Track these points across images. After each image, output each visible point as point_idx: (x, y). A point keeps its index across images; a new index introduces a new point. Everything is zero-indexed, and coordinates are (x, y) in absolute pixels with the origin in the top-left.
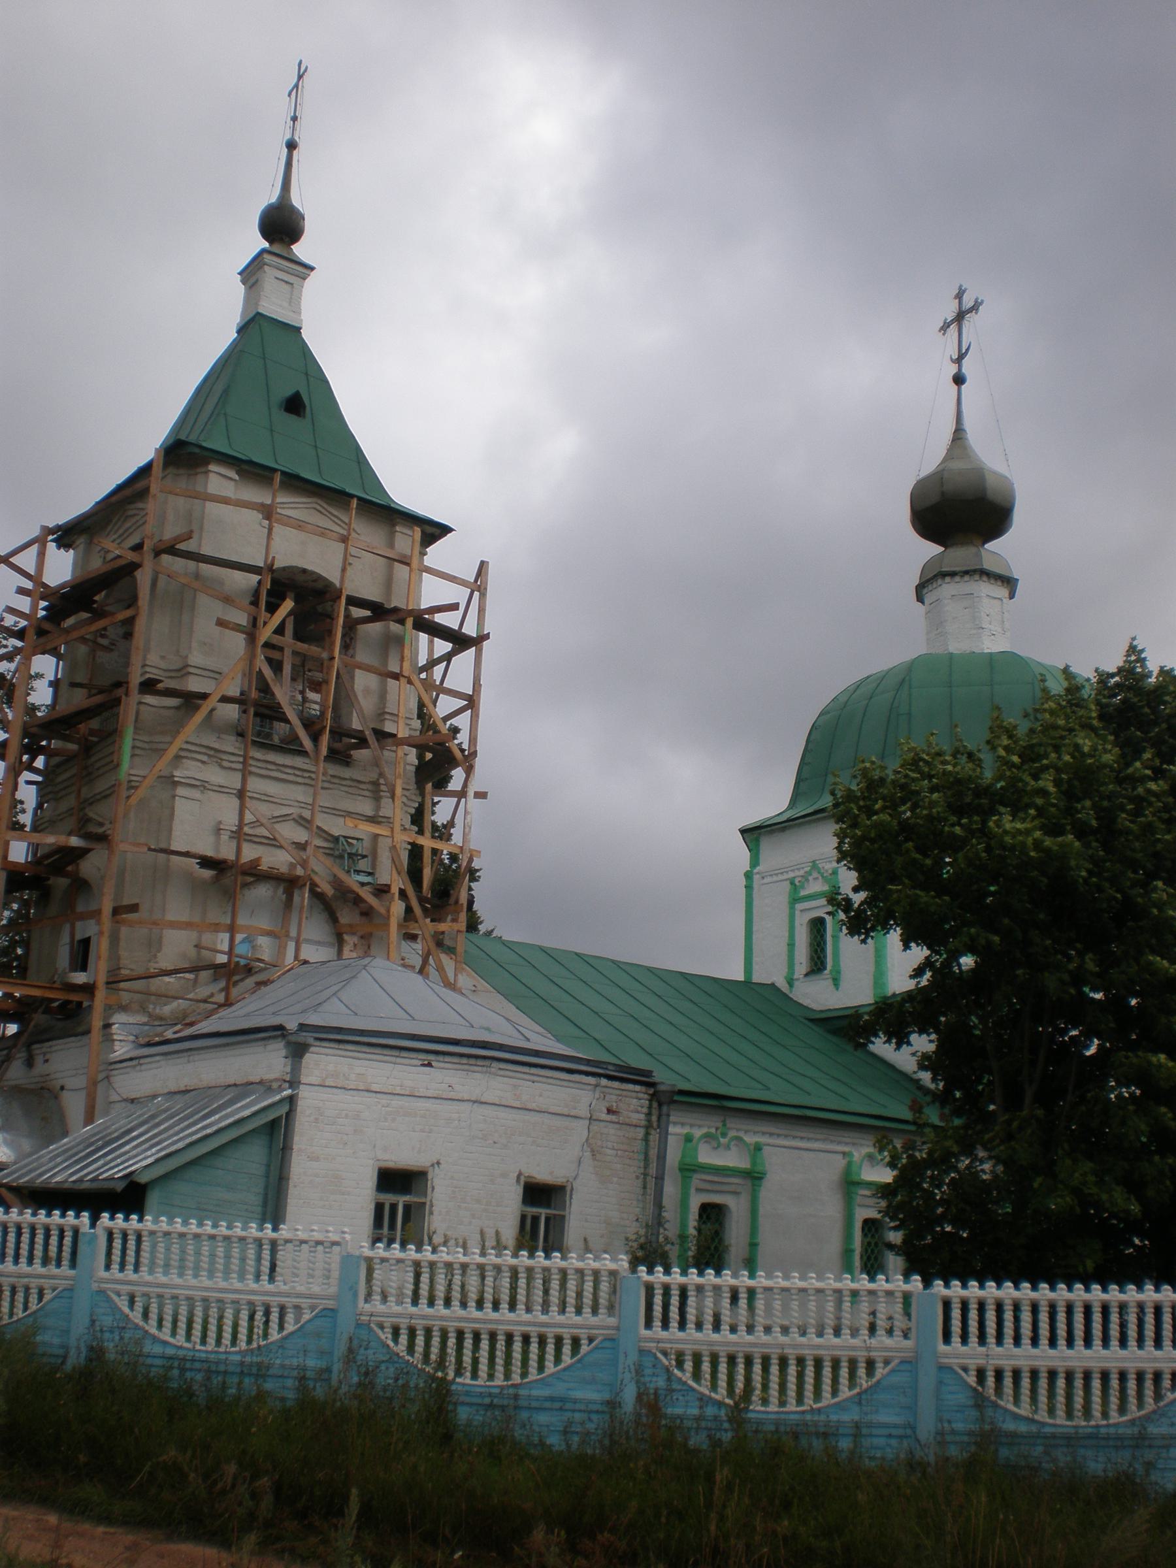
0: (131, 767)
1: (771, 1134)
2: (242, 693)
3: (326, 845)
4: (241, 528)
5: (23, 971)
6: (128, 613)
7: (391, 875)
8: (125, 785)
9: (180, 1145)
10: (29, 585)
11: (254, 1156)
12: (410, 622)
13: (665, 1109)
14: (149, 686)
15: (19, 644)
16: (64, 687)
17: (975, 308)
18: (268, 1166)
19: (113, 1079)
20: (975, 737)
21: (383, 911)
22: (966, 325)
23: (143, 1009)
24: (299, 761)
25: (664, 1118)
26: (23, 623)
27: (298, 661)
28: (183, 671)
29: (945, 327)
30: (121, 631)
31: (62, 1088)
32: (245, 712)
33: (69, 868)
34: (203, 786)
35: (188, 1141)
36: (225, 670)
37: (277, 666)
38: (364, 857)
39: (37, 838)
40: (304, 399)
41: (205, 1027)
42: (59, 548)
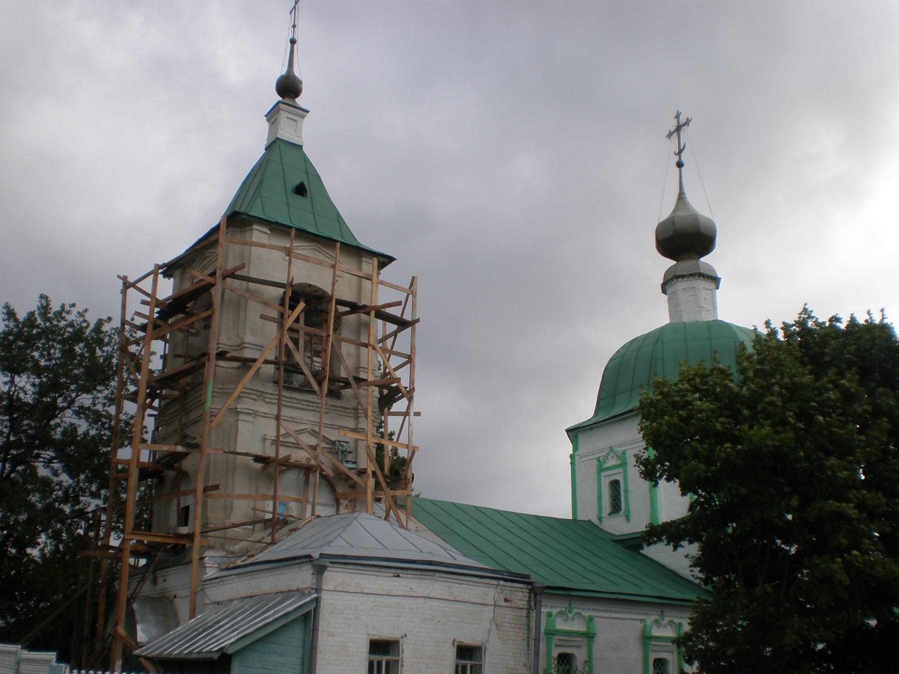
0: (212, 404)
1: (598, 610)
2: (276, 358)
3: (328, 446)
4: (272, 262)
5: (149, 528)
6: (208, 313)
7: (365, 462)
8: (209, 415)
9: (252, 630)
10: (149, 299)
11: (296, 636)
12: (373, 313)
13: (538, 597)
14: (221, 355)
15: (143, 334)
16: (169, 360)
17: (687, 123)
18: (304, 641)
19: (206, 590)
20: (727, 363)
21: (362, 484)
22: (682, 132)
23: (222, 548)
24: (310, 397)
25: (538, 603)
26: (145, 321)
27: (308, 339)
28: (241, 346)
29: (670, 135)
30: (202, 325)
31: (175, 596)
32: (278, 369)
33: (176, 465)
34: (255, 414)
35: (255, 627)
36: (266, 345)
37: (296, 342)
38: (350, 452)
39: (156, 447)
40: (304, 188)
41: (261, 557)
42: (164, 277)
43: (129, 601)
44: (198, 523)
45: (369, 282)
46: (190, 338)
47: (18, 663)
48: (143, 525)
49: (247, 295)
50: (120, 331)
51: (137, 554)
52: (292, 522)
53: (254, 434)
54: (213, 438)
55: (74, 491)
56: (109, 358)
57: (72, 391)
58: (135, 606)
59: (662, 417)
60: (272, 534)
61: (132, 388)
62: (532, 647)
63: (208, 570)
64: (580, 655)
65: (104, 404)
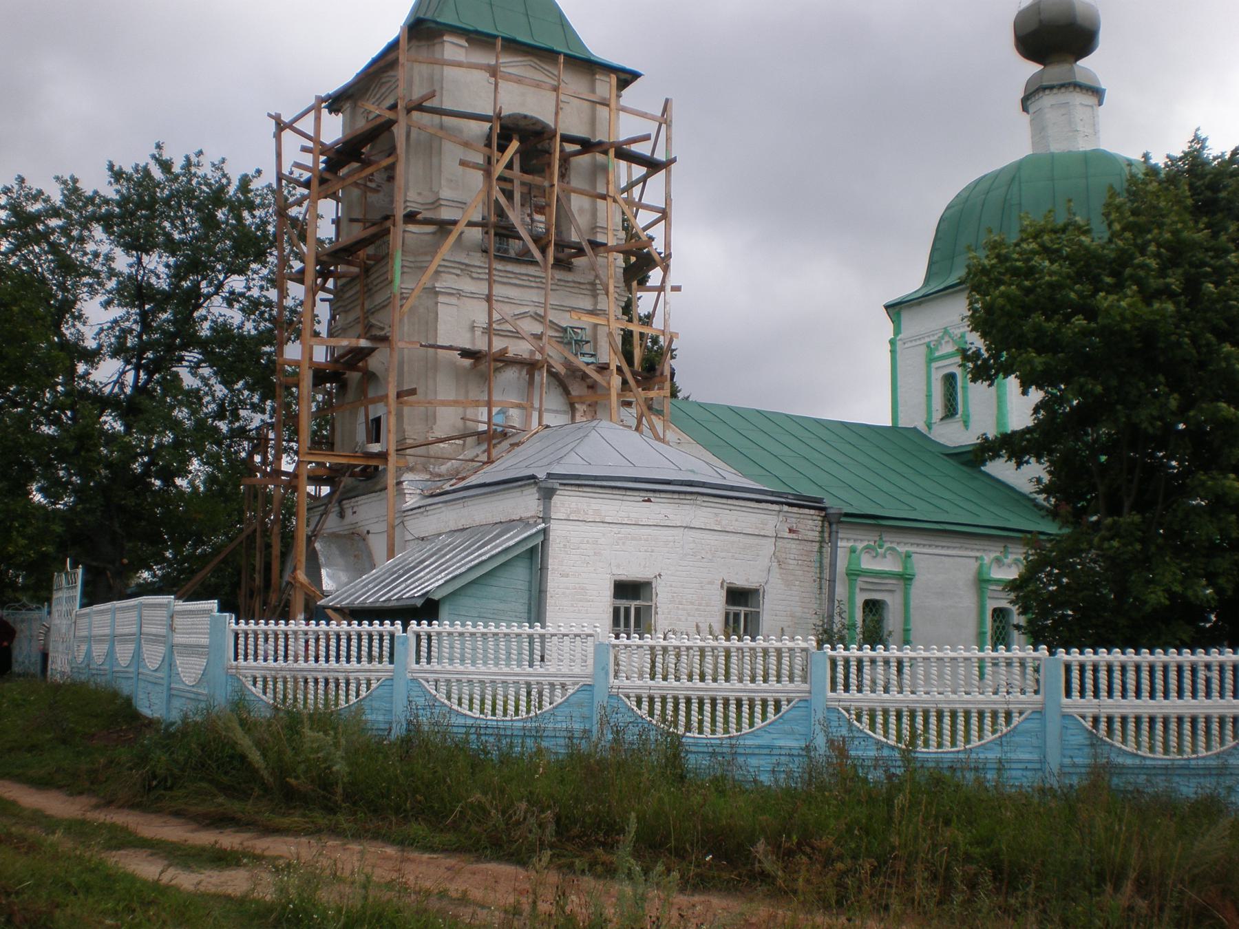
4: (474, 87)
5: (331, 445)
7: (609, 355)
9: (463, 569)
10: (310, 144)
11: (520, 575)
12: (612, 152)
13: (834, 526)
14: (411, 217)
15: (306, 191)
16: (344, 224)
18: (530, 582)
21: (605, 384)
23: (426, 470)
24: (531, 270)
27: (525, 190)
28: (436, 204)
30: (385, 176)
31: (368, 532)
33: (360, 364)
34: (459, 294)
36: (469, 201)
37: (509, 195)
38: (587, 342)
39: (333, 342)
43: (310, 540)
44: (393, 438)
45: (606, 109)
46: (369, 194)
47: (172, 617)
48: (321, 443)
49: (440, 134)
50: (277, 192)
51: (316, 480)
52: (514, 435)
53: (459, 319)
54: (406, 329)
55: (231, 403)
56: (264, 223)
57: (219, 271)
58: (317, 546)
59: (997, 287)
60: (488, 451)
61: (297, 265)
62: (826, 590)
63: (408, 498)
64: (892, 602)
65: (262, 288)
